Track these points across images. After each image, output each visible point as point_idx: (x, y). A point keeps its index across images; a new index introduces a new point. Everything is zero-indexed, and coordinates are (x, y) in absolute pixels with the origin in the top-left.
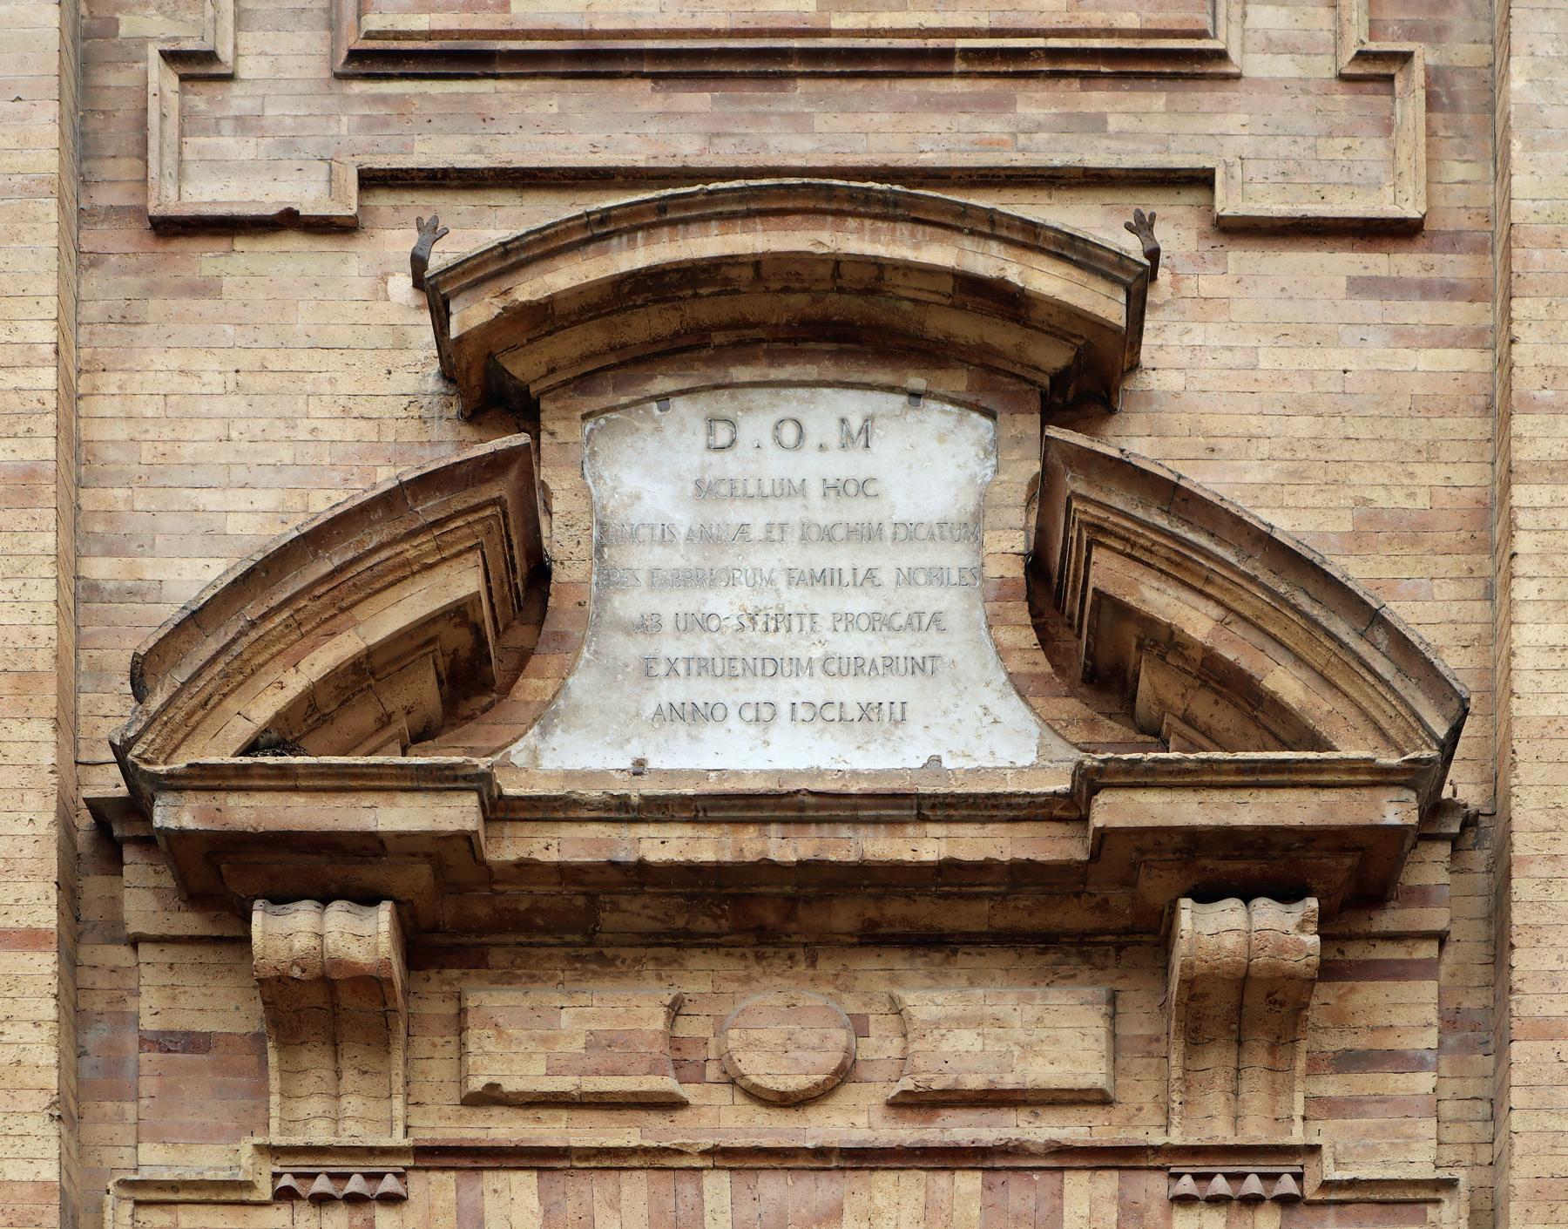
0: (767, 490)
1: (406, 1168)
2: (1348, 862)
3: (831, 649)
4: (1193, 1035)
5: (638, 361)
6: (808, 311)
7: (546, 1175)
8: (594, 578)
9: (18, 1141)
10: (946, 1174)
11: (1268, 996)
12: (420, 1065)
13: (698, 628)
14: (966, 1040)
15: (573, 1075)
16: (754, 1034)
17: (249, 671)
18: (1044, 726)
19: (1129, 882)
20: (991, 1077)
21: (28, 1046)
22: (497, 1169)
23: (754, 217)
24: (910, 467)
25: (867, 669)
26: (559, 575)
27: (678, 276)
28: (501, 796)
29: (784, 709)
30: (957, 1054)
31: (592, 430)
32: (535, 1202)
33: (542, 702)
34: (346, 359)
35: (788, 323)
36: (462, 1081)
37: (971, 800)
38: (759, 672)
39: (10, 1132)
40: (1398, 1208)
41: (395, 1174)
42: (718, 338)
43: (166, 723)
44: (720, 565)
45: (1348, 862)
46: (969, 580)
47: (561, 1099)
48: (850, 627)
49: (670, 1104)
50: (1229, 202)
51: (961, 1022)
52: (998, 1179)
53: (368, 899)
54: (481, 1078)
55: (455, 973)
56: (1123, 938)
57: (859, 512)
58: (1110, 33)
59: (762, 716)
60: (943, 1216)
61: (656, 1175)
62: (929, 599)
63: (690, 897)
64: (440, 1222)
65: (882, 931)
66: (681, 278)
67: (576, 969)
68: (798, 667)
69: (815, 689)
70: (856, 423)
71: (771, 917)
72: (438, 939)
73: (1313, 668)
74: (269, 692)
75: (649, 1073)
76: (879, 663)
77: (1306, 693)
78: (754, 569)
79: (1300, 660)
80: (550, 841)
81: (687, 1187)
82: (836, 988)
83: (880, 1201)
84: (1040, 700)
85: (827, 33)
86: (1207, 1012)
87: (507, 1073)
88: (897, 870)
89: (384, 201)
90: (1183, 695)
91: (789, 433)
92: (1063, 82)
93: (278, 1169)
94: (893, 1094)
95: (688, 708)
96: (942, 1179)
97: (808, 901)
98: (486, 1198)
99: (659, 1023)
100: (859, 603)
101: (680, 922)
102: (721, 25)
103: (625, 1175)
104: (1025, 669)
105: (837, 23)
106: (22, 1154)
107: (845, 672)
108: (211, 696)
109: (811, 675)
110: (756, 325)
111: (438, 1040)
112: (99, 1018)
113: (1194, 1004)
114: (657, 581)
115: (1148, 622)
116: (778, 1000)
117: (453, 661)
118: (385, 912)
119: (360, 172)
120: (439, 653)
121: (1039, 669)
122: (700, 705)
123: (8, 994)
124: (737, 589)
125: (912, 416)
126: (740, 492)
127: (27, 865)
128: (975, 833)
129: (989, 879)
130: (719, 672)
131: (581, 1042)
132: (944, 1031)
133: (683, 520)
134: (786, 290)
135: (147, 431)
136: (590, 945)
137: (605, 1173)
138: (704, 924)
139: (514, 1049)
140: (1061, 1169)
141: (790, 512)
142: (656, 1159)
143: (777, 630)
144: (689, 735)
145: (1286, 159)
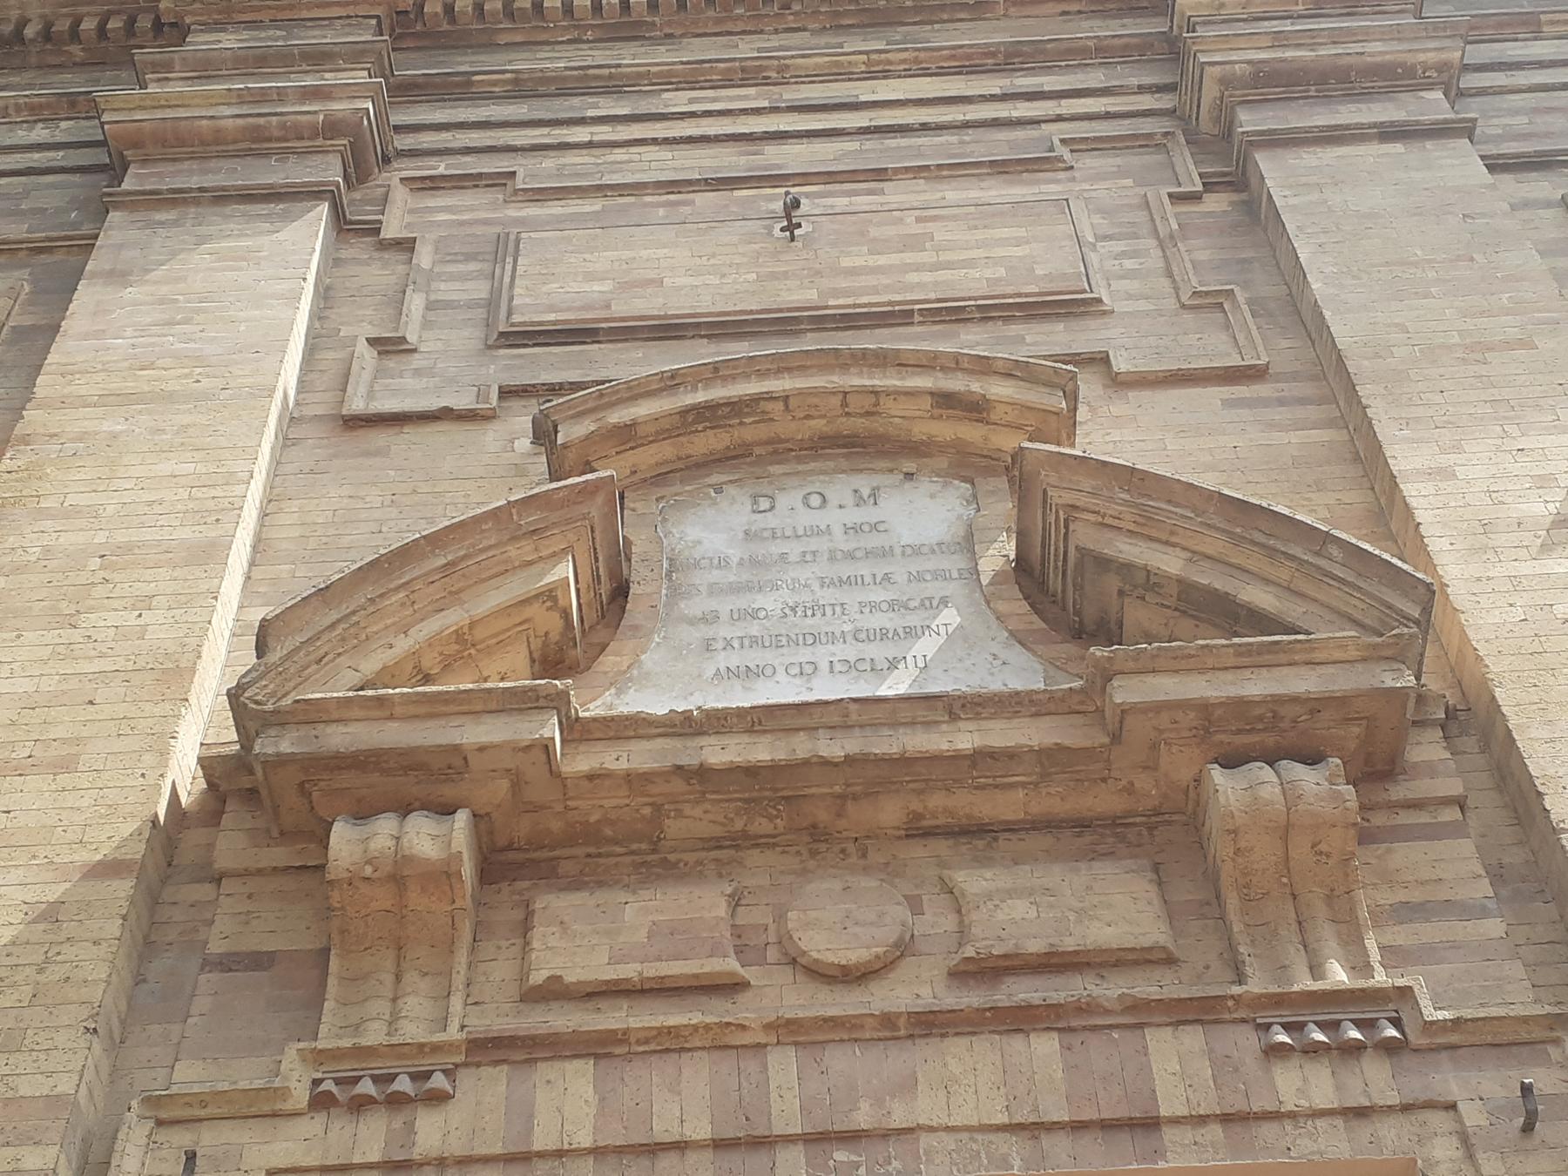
0: (801, 532)
1: (457, 1066)
2: (1356, 730)
3: (859, 625)
4: (1245, 891)
5: (698, 466)
6: (825, 429)
7: (603, 1063)
8: (664, 592)
9: (42, 1056)
10: (1020, 1036)
11: (1312, 848)
12: (482, 967)
13: (749, 617)
14: (1020, 909)
15: (635, 962)
16: (813, 914)
17: (364, 637)
18: (1047, 664)
19: (1150, 767)
20: (1051, 941)
21: (81, 964)
22: (551, 1058)
23: (782, 372)
24: (911, 513)
25: (890, 636)
26: (634, 589)
27: (728, 409)
28: (578, 719)
29: (824, 666)
30: (1014, 922)
31: (663, 507)
32: (590, 1091)
33: (619, 671)
34: (478, 484)
35: (811, 439)
36: (523, 976)
37: (997, 699)
38: (801, 642)
39: (37, 1047)
40: (1514, 1049)
41: (443, 1071)
42: (758, 450)
43: (280, 673)
44: (766, 578)
45: (1356, 730)
46: (968, 576)
47: (622, 987)
48: (874, 610)
49: (731, 987)
51: (1011, 893)
52: (1075, 1040)
53: (446, 810)
54: (542, 972)
55: (526, 884)
56: (1154, 819)
57: (874, 541)
58: (1019, 295)
60: (1025, 1080)
61: (716, 1054)
62: (935, 589)
63: (746, 801)
64: (487, 1118)
65: (925, 823)
66: (732, 410)
67: (641, 873)
68: (832, 638)
69: (850, 651)
70: (866, 492)
71: (823, 815)
72: (511, 856)
73: (1279, 585)
74: (379, 651)
75: (711, 956)
76: (900, 631)
77: (1280, 602)
78: (793, 579)
79: (1267, 581)
80: (620, 753)
81: (751, 1065)
82: (888, 874)
83: (954, 1067)
84: (1041, 647)
85: (826, 307)
86: (1255, 866)
87: (569, 965)
88: (934, 759)
89: (515, 404)
90: (1166, 625)
91: (815, 501)
92: (990, 323)
93: (320, 1075)
94: (954, 962)
95: (743, 669)
96: (1017, 1043)
97: (855, 797)
98: (538, 1090)
99: (722, 910)
100: (879, 595)
101: (739, 825)
102: (754, 308)
103: (686, 1056)
104: (1022, 627)
105: (831, 303)
106: (43, 1069)
107: (872, 638)
108: (326, 654)
109: (845, 642)
110: (787, 441)
111: (504, 944)
112: (168, 947)
113: (1240, 860)
114: (714, 590)
115: (1126, 568)
116: (837, 885)
117: (545, 645)
118: (462, 818)
119: (500, 387)
120: (531, 632)
121: (1035, 627)
122: (752, 666)
123: (75, 918)
124: (780, 592)
125: (908, 485)
126: (779, 535)
127: (129, 809)
128: (1004, 726)
129: (1020, 770)
130: (767, 644)
131: (644, 933)
132: (998, 902)
133: (735, 554)
134: (808, 417)
135: (316, 531)
136: (654, 851)
137: (665, 1056)
138: (761, 826)
139: (578, 943)
140: (1140, 1026)
141: (821, 544)
142: (720, 1041)
143: (813, 615)
144: (743, 687)
145: (1157, 347)
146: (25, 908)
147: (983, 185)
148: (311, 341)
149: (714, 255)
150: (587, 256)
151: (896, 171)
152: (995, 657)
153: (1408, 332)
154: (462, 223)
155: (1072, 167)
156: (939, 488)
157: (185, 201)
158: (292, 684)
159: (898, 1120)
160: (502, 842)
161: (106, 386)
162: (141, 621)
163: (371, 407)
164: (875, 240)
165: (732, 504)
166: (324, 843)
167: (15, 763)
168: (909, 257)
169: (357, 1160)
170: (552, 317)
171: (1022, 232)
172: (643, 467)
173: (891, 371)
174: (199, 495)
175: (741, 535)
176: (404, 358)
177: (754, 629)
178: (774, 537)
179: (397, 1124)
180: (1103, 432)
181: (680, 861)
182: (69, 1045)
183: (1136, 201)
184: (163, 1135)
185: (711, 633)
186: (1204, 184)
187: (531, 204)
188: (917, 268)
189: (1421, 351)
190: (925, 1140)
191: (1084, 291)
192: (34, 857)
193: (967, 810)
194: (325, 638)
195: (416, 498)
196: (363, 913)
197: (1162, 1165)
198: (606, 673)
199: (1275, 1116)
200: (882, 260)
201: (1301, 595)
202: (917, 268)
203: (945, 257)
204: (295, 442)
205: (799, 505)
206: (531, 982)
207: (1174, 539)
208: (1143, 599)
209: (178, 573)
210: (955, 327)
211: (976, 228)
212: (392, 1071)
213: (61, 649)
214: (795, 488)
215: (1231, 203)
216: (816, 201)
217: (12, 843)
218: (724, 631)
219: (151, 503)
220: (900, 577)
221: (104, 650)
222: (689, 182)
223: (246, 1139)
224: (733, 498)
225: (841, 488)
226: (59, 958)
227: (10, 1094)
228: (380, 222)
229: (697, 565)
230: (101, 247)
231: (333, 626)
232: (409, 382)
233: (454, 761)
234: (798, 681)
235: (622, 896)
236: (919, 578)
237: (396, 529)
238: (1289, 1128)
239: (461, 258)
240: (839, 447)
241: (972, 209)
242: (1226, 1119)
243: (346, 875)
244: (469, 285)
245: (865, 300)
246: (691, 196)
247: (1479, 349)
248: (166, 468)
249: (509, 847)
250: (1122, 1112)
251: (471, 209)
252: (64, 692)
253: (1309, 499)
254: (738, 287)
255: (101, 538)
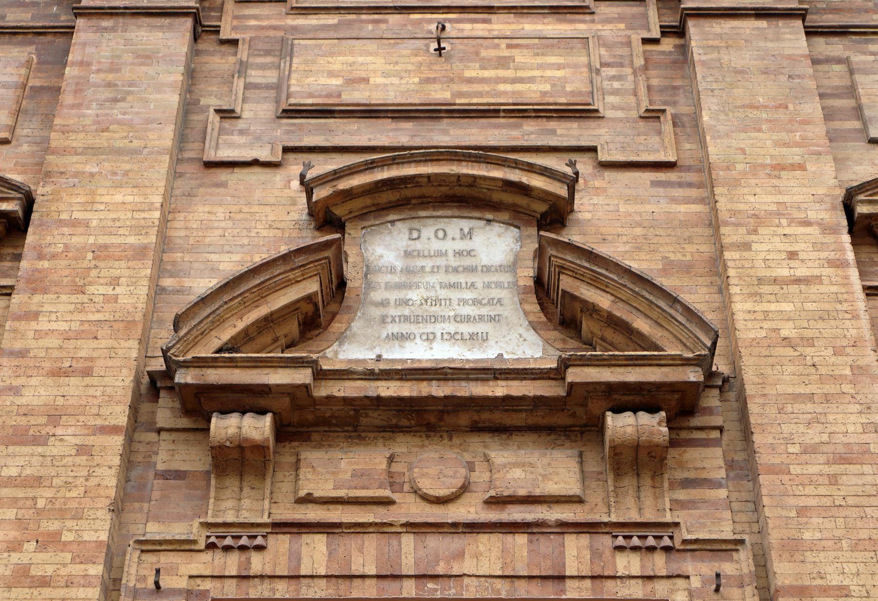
0: (432, 254)
1: (267, 533)
2: (676, 396)
3: (457, 312)
5: (383, 209)
6: (448, 192)
7: (331, 536)
9: (92, 522)
10: (511, 535)
12: (278, 485)
16: (425, 470)
19: (584, 405)
20: (529, 490)
26: (350, 284)
28: (321, 370)
29: (439, 335)
30: (514, 479)
35: (440, 197)
36: (296, 491)
42: (414, 201)
45: (676, 396)
46: (512, 286)
49: (387, 502)
50: (603, 156)
51: (515, 465)
53: (262, 412)
55: (297, 444)
56: (583, 429)
57: (468, 262)
58: (556, 104)
59: (430, 338)
61: (380, 536)
62: (496, 293)
63: (398, 411)
65: (480, 425)
68: (444, 319)
69: (451, 327)
70: (466, 230)
71: (433, 420)
72: (290, 429)
76: (477, 317)
79: (646, 316)
81: (394, 542)
83: (482, 548)
85: (455, 104)
89: (291, 157)
91: (441, 234)
93: (209, 534)
95: (400, 335)
96: (509, 538)
97: (448, 413)
100: (468, 295)
101: (394, 421)
103: (366, 535)
104: (536, 320)
108: (205, 330)
109: (450, 322)
110: (428, 197)
111: (287, 474)
114: (388, 287)
115: (584, 302)
117: (306, 317)
118: (268, 418)
121: (541, 320)
122: (404, 334)
124: (420, 290)
125: (488, 228)
127: (118, 398)
128: (518, 384)
129: (525, 403)
130: (412, 321)
133: (399, 264)
134: (440, 185)
136: (355, 431)
138: (404, 422)
139: (320, 477)
140: (563, 533)
141: (441, 262)
142: (381, 528)
143: (436, 305)
145: (623, 143)
146: (76, 447)
147: (546, 21)
148: (186, 107)
149: (397, 63)
150: (330, 59)
151: (499, 8)
152: (521, 336)
153: (745, 154)
154: (263, 28)
155: (593, 13)
156: (503, 231)
157: (117, 14)
158: (191, 346)
159: (456, 571)
160: (285, 423)
161: (86, 142)
162: (115, 292)
163: (218, 155)
164: (483, 59)
165: (399, 233)
166: (209, 421)
167: (64, 370)
168: (501, 73)
169: (227, 574)
170: (310, 101)
171: (561, 60)
172: (355, 210)
173: (483, 166)
174: (137, 216)
175: (402, 253)
176: (234, 121)
177: (406, 311)
178: (419, 256)
179: (243, 559)
180: (589, 197)
181: (367, 436)
182: (103, 517)
183: (624, 40)
184: (145, 557)
185: (385, 313)
186: (662, 32)
187: (301, 16)
188: (505, 80)
189: (750, 167)
190: (466, 580)
191: (589, 104)
192: (78, 421)
193: (499, 421)
194: (205, 322)
195: (241, 216)
196: (225, 459)
197: (564, 597)
198: (334, 333)
199: (614, 577)
200: (486, 74)
201: (662, 326)
202: (505, 80)
203: (521, 74)
204: (180, 175)
205: (432, 236)
206: (300, 495)
207: (607, 290)
208: (591, 315)
209: (131, 264)
210: (520, 120)
211: (538, 55)
212: (240, 534)
213: (79, 306)
214: (431, 225)
215: (675, 46)
216: (455, 25)
217: (68, 413)
218: (393, 311)
219: (114, 220)
220: (479, 285)
221: (99, 308)
222: (386, 8)
223: (179, 561)
224: (400, 230)
225: (456, 226)
226: (94, 474)
227: (80, 539)
228: (219, 27)
229: (380, 270)
230: (75, 44)
231: (208, 316)
232: (236, 138)
233: (265, 390)
234: (426, 343)
235: (340, 455)
236: (488, 286)
237: (231, 235)
238: (619, 583)
239: (262, 53)
240: (455, 202)
241: (537, 41)
242: (593, 577)
243: (218, 444)
244: (268, 73)
245: (475, 101)
246: (387, 17)
247: (780, 167)
248: (119, 198)
249: (289, 425)
250: (550, 573)
251: (268, 17)
252: (83, 331)
253: (683, 248)
254: (409, 86)
255: (91, 240)
